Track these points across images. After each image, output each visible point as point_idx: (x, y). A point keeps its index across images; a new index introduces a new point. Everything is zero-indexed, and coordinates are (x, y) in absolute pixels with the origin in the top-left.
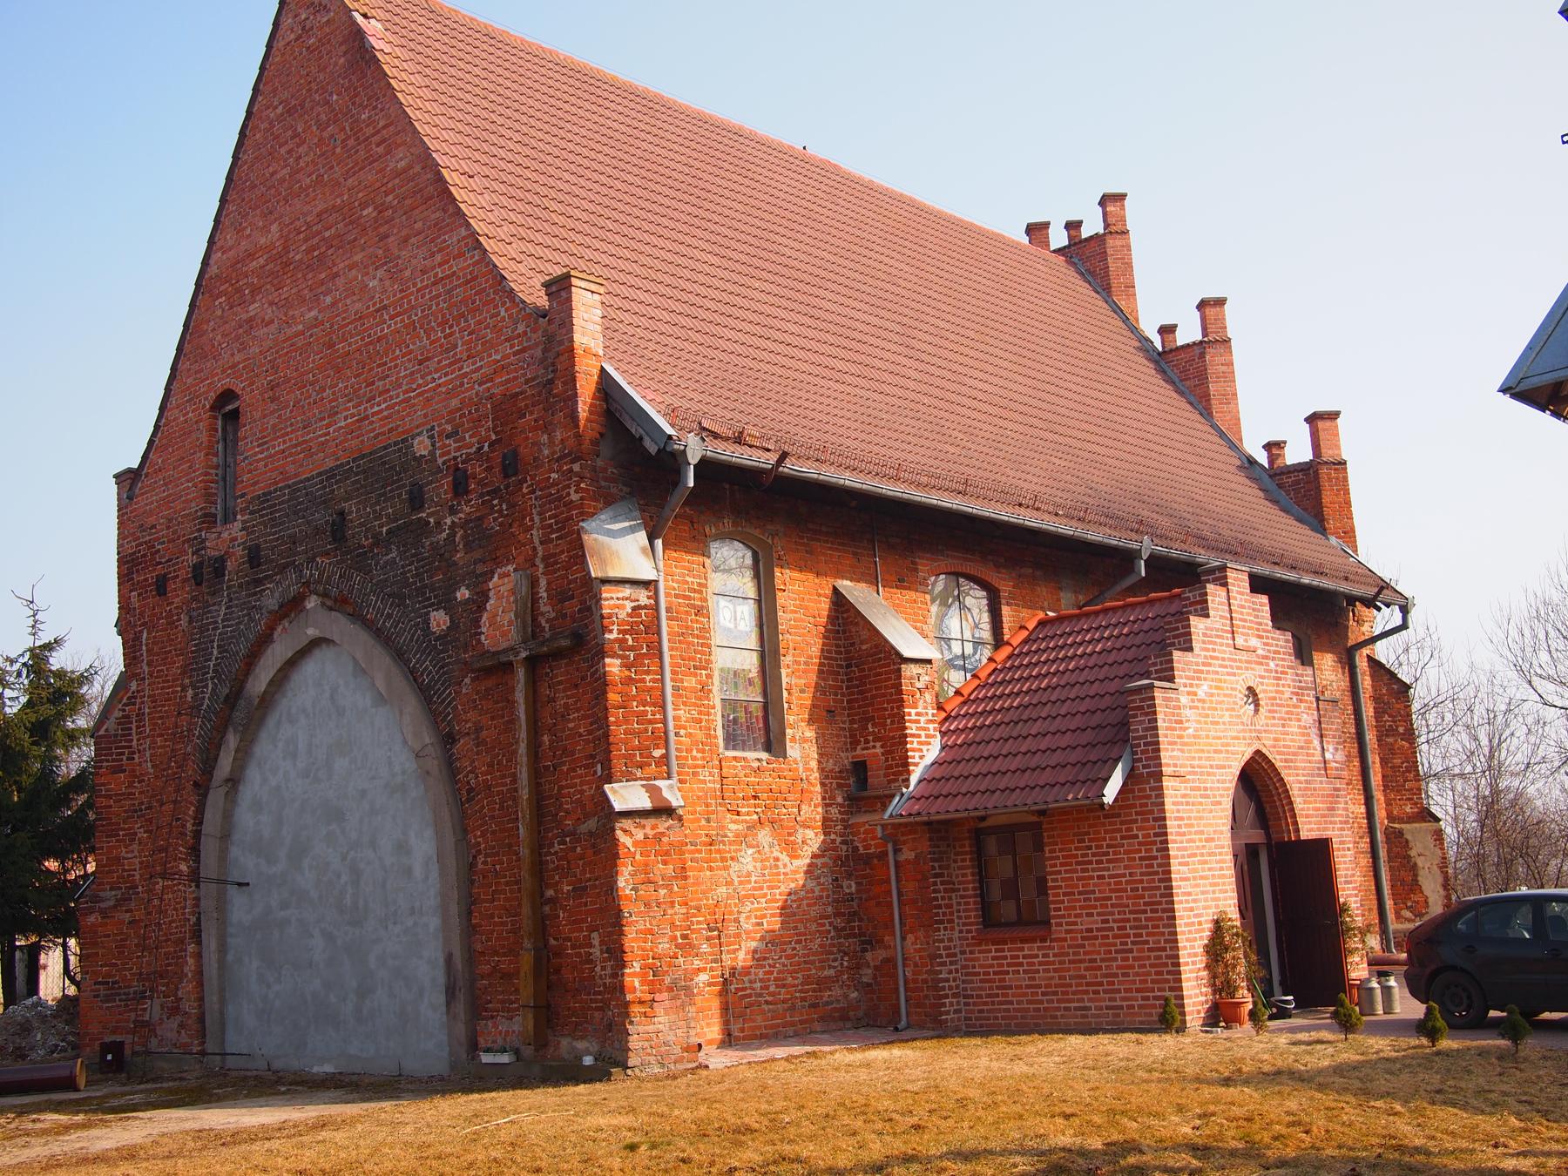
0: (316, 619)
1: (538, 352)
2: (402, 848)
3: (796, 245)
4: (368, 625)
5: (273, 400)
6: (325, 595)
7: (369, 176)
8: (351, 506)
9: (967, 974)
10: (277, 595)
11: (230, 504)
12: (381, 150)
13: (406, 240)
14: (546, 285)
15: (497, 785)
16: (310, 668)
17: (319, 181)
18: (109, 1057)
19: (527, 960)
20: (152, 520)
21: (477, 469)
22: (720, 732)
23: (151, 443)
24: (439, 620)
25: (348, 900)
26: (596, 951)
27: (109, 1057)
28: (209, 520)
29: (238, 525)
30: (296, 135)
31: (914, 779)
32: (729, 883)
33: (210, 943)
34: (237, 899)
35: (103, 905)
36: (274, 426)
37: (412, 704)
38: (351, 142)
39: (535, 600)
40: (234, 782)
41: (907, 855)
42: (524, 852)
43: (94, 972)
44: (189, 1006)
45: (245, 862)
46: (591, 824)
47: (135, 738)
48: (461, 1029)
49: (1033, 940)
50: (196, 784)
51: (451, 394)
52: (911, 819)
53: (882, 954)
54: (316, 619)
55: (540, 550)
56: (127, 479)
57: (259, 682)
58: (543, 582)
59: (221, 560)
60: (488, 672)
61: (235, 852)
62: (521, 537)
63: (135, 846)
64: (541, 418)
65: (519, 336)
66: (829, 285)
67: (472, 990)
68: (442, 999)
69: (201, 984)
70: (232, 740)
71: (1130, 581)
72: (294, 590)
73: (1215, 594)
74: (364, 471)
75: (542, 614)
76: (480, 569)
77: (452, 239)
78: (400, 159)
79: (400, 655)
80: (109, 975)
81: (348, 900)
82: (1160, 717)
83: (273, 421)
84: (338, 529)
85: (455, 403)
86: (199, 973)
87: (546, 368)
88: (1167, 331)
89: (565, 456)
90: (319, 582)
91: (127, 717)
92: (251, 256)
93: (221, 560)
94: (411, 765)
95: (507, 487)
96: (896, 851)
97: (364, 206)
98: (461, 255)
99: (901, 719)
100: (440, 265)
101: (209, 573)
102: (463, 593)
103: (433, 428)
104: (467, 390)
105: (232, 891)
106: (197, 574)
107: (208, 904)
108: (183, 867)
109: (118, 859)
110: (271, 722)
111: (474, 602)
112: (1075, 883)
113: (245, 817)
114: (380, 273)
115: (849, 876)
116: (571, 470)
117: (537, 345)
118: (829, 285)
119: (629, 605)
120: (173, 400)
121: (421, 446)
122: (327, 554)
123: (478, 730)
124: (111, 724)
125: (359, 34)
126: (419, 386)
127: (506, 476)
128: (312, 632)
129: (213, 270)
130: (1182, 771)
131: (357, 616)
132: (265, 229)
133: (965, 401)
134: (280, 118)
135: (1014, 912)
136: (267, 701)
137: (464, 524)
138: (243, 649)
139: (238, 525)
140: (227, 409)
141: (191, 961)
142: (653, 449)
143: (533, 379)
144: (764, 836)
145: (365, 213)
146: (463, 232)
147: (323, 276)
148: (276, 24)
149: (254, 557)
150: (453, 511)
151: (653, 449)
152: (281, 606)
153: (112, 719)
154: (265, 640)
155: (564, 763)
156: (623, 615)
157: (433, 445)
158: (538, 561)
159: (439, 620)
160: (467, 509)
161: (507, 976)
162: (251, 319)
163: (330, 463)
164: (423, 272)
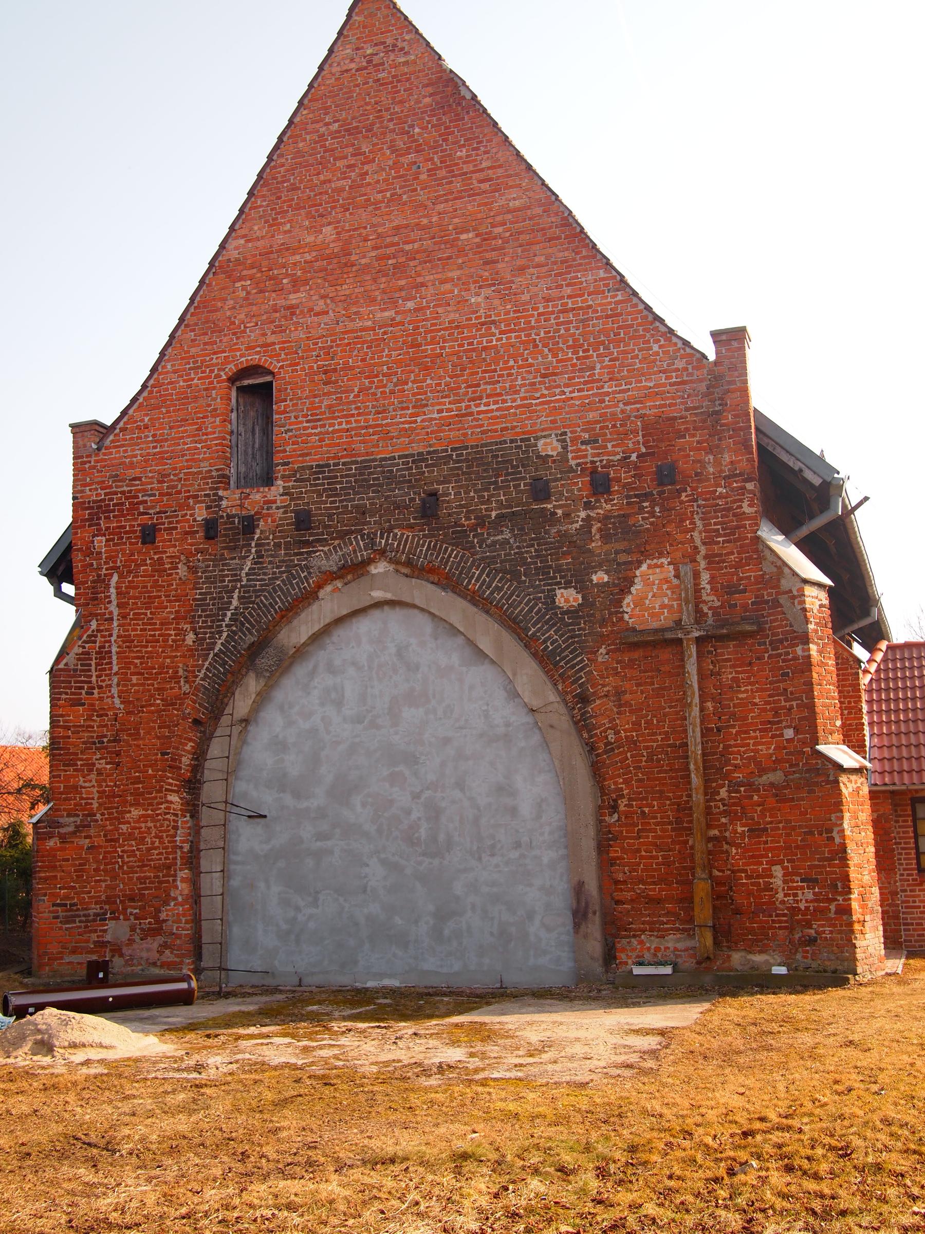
1: (703, 387)
2: (503, 789)
9: (907, 907)
10: (335, 557)
12: (485, 186)
13: (522, 269)
15: (644, 741)
18: (101, 975)
25: (423, 832)
27: (101, 975)
35: (62, 830)
36: (330, 407)
38: (442, 173)
39: (698, 590)
43: (53, 895)
47: (94, 674)
50: (197, 722)
51: (590, 407)
52: (883, 788)
55: (703, 550)
56: (87, 434)
58: (705, 577)
62: (679, 537)
63: (93, 776)
64: (706, 441)
65: (677, 370)
74: (467, 460)
75: (705, 602)
80: (67, 897)
81: (423, 832)
84: (430, 507)
86: (196, 897)
87: (713, 401)
89: (736, 475)
91: (88, 653)
95: (660, 493)
100: (569, 297)
103: (565, 433)
104: (607, 407)
109: (76, 788)
111: (615, 585)
114: (485, 292)
116: (744, 488)
117: (701, 381)
121: (549, 446)
122: (411, 527)
124: (70, 659)
126: (543, 396)
127: (661, 484)
134: (335, 135)
136: (301, 652)
143: (695, 408)
145: (464, 237)
147: (402, 282)
149: (303, 521)
152: (340, 569)
153: (72, 655)
155: (733, 726)
157: (565, 448)
158: (699, 558)
159: (567, 597)
160: (608, 507)
163: (417, 448)
164: (547, 300)
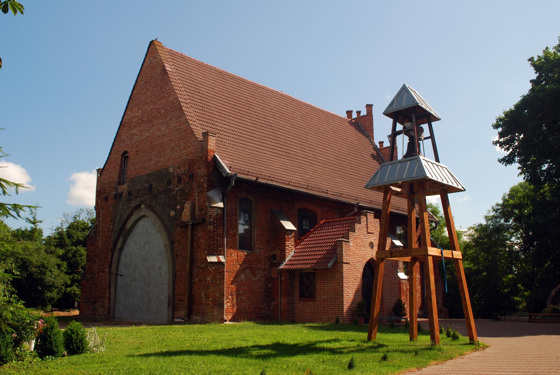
0: (144, 210)
3: (274, 120)
4: (155, 213)
5: (137, 155)
6: (146, 205)
7: (163, 102)
8: (153, 183)
11: (125, 179)
14: (203, 133)
16: (141, 222)
17: (152, 101)
19: (187, 296)
20: (105, 182)
21: (184, 177)
22: (238, 245)
23: (106, 162)
24: (172, 213)
26: (203, 296)
28: (119, 184)
29: (126, 185)
30: (147, 89)
31: (287, 260)
32: (238, 282)
33: (113, 290)
34: (120, 279)
37: (164, 234)
39: (195, 210)
40: (121, 250)
41: (283, 278)
42: (188, 270)
44: (107, 305)
45: (122, 270)
46: (204, 265)
48: (171, 313)
49: (311, 301)
50: (112, 250)
53: (276, 302)
54: (144, 210)
57: (129, 225)
58: (197, 206)
59: (122, 194)
60: (183, 227)
61: (120, 267)
66: (282, 131)
67: (173, 305)
68: (167, 306)
69: (109, 300)
70: (121, 239)
71: (353, 213)
72: (138, 203)
73: (363, 219)
76: (183, 201)
77: (182, 120)
78: (171, 98)
79: (162, 221)
82: (344, 248)
83: (136, 160)
84: (150, 188)
85: (180, 160)
86: (109, 297)
88: (381, 143)
90: (145, 201)
92: (134, 118)
93: (122, 194)
94: (164, 248)
96: (281, 277)
97: (162, 109)
98: (184, 124)
99: (284, 245)
101: (118, 196)
102: (178, 207)
105: (133, 169)
106: (115, 197)
107: (113, 280)
108: (107, 270)
110: (131, 235)
112: (322, 287)
113: (123, 259)
114: (165, 126)
115: (269, 283)
118: (282, 131)
119: (216, 213)
120: (112, 152)
121: (171, 170)
123: (180, 240)
125: (164, 66)
128: (142, 213)
129: (124, 120)
130: (348, 262)
131: (153, 210)
132: (138, 112)
133: (316, 163)
135: (307, 293)
137: (180, 190)
138: (125, 216)
139: (126, 185)
140: (125, 156)
141: (108, 294)
142: (225, 176)
144: (248, 271)
146: (185, 118)
148: (144, 60)
149: (130, 193)
150: (177, 187)
151: (225, 176)
154: (131, 215)
156: (214, 215)
159: (172, 213)
161: (183, 301)
162: (133, 134)
163: (149, 172)
